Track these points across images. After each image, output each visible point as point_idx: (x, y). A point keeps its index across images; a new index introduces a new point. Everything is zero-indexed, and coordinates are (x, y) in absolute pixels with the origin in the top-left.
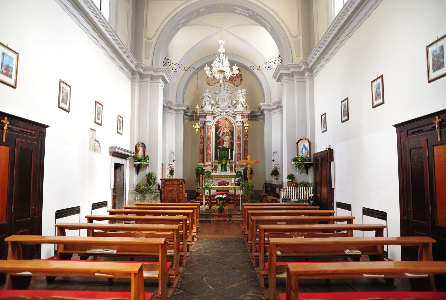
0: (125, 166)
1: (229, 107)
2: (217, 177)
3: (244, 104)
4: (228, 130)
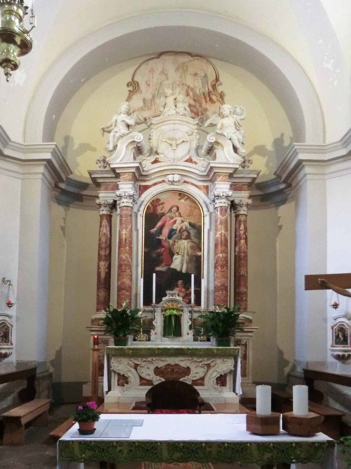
1: (190, 160)
4: (186, 224)
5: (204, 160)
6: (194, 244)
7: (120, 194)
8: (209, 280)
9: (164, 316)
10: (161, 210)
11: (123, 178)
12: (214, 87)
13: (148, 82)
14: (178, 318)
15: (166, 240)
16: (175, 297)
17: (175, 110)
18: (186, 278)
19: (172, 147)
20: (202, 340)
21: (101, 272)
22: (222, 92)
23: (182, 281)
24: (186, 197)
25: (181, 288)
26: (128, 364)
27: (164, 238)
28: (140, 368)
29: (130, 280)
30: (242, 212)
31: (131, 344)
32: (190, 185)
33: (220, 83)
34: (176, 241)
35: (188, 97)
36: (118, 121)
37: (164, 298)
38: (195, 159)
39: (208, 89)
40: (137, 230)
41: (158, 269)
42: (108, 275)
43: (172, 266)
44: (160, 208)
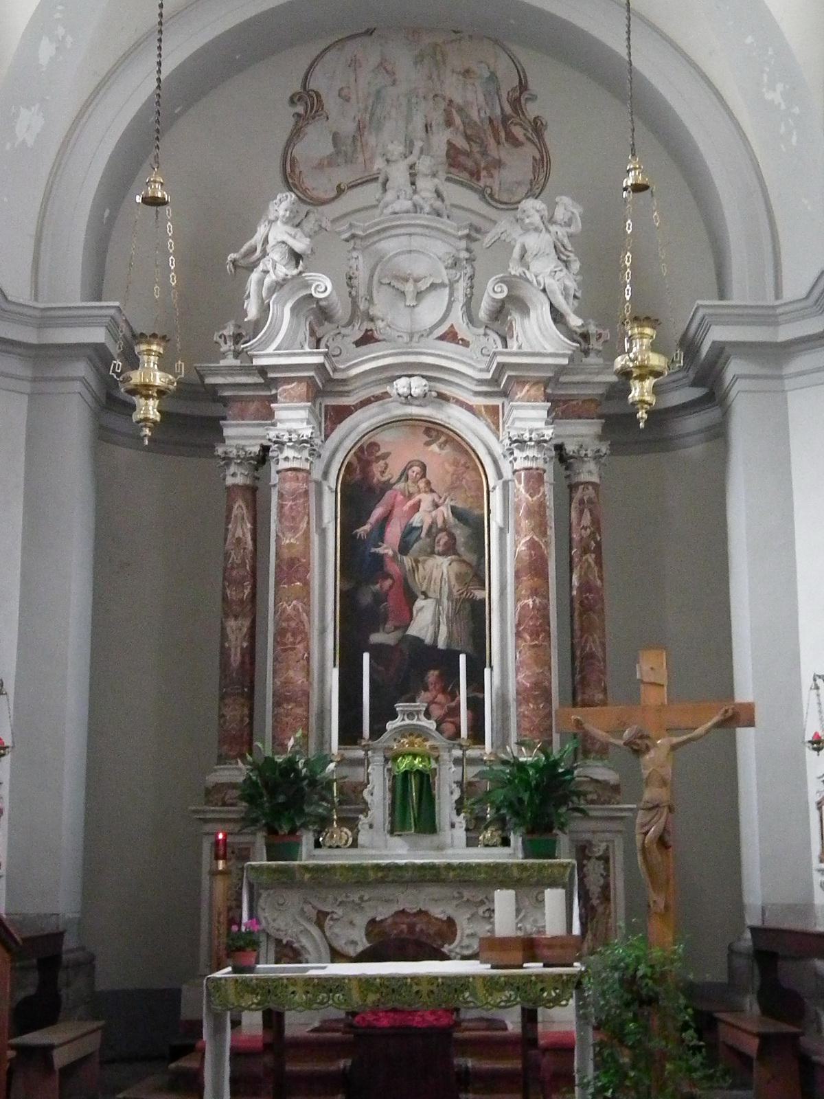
1: (451, 336)
2: (362, 877)
4: (445, 511)
5: (485, 335)
6: (464, 569)
7: (277, 437)
8: (506, 669)
9: (390, 774)
10: (383, 473)
11: (285, 390)
12: (516, 104)
13: (345, 92)
14: (426, 781)
15: (394, 557)
16: (418, 719)
17: (411, 199)
19: (405, 301)
20: (490, 843)
21: (229, 648)
22: (535, 118)
23: (436, 673)
24: (443, 439)
25: (434, 693)
26: (302, 911)
27: (390, 553)
28: (332, 923)
29: (304, 674)
30: (584, 477)
31: (308, 855)
32: (454, 406)
33: (529, 96)
34: (421, 559)
35: (452, 129)
36: (271, 241)
37: (390, 722)
38: (463, 330)
39: (502, 109)
40: (323, 532)
41: (376, 638)
42: (247, 660)
43: (413, 631)
44: (380, 469)
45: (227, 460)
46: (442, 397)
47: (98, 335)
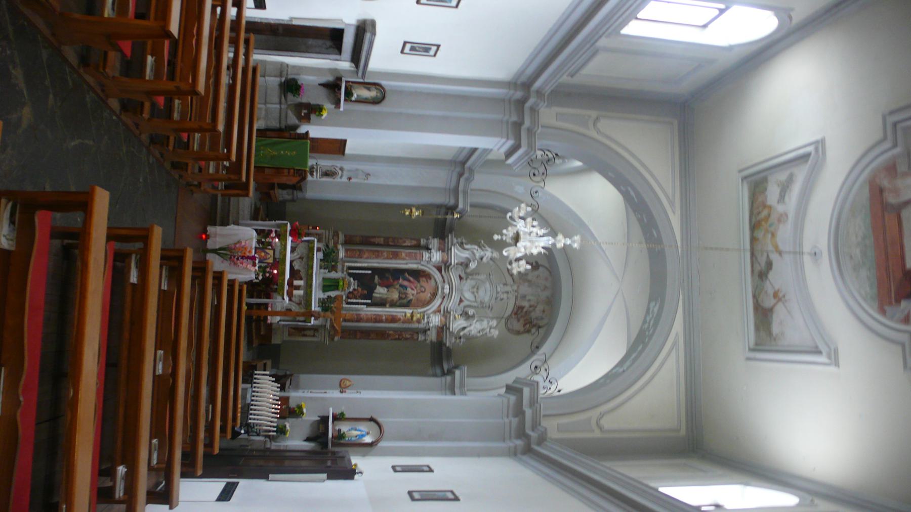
0: (337, 57)
1: (461, 301)
3: (466, 331)
4: (411, 297)
18: (369, 296)
38: (462, 305)
45: (428, 239)
46: (444, 298)
47: (461, 206)
